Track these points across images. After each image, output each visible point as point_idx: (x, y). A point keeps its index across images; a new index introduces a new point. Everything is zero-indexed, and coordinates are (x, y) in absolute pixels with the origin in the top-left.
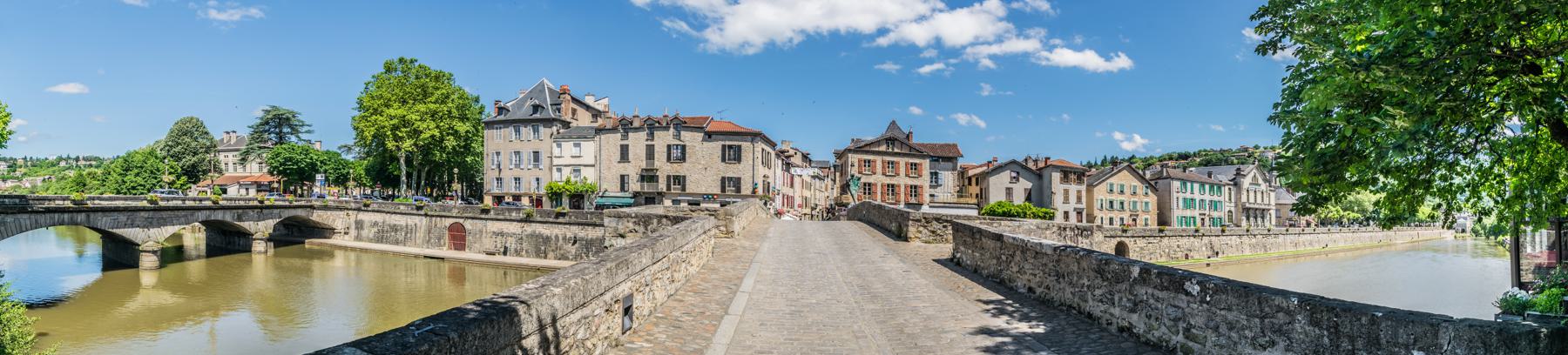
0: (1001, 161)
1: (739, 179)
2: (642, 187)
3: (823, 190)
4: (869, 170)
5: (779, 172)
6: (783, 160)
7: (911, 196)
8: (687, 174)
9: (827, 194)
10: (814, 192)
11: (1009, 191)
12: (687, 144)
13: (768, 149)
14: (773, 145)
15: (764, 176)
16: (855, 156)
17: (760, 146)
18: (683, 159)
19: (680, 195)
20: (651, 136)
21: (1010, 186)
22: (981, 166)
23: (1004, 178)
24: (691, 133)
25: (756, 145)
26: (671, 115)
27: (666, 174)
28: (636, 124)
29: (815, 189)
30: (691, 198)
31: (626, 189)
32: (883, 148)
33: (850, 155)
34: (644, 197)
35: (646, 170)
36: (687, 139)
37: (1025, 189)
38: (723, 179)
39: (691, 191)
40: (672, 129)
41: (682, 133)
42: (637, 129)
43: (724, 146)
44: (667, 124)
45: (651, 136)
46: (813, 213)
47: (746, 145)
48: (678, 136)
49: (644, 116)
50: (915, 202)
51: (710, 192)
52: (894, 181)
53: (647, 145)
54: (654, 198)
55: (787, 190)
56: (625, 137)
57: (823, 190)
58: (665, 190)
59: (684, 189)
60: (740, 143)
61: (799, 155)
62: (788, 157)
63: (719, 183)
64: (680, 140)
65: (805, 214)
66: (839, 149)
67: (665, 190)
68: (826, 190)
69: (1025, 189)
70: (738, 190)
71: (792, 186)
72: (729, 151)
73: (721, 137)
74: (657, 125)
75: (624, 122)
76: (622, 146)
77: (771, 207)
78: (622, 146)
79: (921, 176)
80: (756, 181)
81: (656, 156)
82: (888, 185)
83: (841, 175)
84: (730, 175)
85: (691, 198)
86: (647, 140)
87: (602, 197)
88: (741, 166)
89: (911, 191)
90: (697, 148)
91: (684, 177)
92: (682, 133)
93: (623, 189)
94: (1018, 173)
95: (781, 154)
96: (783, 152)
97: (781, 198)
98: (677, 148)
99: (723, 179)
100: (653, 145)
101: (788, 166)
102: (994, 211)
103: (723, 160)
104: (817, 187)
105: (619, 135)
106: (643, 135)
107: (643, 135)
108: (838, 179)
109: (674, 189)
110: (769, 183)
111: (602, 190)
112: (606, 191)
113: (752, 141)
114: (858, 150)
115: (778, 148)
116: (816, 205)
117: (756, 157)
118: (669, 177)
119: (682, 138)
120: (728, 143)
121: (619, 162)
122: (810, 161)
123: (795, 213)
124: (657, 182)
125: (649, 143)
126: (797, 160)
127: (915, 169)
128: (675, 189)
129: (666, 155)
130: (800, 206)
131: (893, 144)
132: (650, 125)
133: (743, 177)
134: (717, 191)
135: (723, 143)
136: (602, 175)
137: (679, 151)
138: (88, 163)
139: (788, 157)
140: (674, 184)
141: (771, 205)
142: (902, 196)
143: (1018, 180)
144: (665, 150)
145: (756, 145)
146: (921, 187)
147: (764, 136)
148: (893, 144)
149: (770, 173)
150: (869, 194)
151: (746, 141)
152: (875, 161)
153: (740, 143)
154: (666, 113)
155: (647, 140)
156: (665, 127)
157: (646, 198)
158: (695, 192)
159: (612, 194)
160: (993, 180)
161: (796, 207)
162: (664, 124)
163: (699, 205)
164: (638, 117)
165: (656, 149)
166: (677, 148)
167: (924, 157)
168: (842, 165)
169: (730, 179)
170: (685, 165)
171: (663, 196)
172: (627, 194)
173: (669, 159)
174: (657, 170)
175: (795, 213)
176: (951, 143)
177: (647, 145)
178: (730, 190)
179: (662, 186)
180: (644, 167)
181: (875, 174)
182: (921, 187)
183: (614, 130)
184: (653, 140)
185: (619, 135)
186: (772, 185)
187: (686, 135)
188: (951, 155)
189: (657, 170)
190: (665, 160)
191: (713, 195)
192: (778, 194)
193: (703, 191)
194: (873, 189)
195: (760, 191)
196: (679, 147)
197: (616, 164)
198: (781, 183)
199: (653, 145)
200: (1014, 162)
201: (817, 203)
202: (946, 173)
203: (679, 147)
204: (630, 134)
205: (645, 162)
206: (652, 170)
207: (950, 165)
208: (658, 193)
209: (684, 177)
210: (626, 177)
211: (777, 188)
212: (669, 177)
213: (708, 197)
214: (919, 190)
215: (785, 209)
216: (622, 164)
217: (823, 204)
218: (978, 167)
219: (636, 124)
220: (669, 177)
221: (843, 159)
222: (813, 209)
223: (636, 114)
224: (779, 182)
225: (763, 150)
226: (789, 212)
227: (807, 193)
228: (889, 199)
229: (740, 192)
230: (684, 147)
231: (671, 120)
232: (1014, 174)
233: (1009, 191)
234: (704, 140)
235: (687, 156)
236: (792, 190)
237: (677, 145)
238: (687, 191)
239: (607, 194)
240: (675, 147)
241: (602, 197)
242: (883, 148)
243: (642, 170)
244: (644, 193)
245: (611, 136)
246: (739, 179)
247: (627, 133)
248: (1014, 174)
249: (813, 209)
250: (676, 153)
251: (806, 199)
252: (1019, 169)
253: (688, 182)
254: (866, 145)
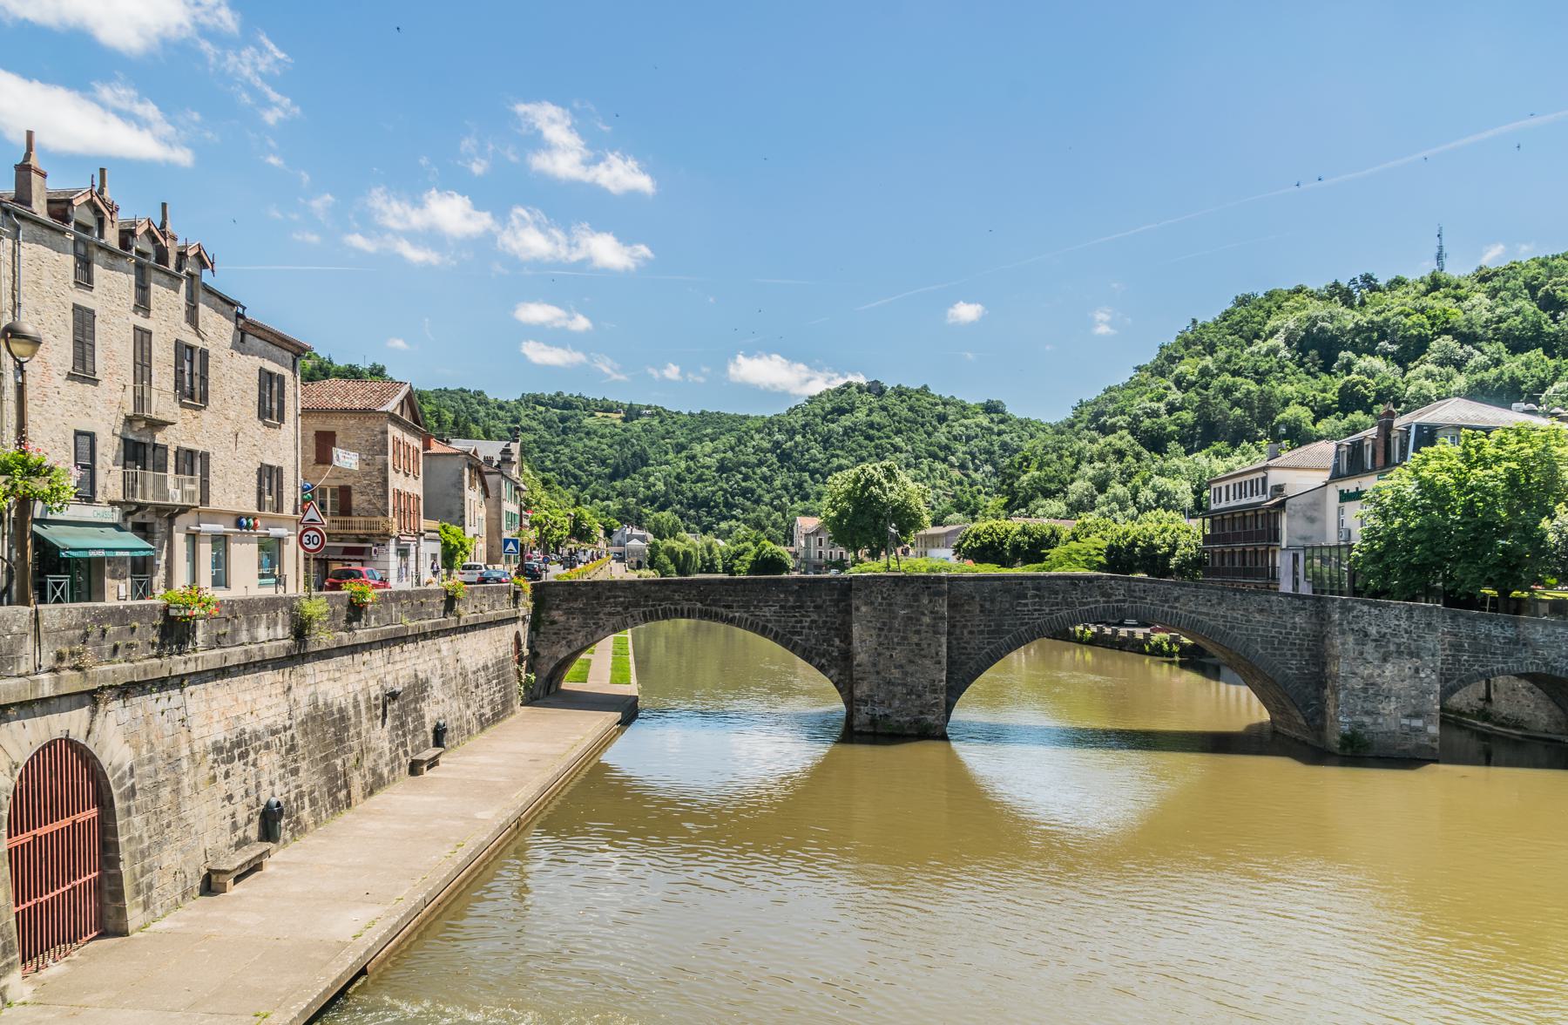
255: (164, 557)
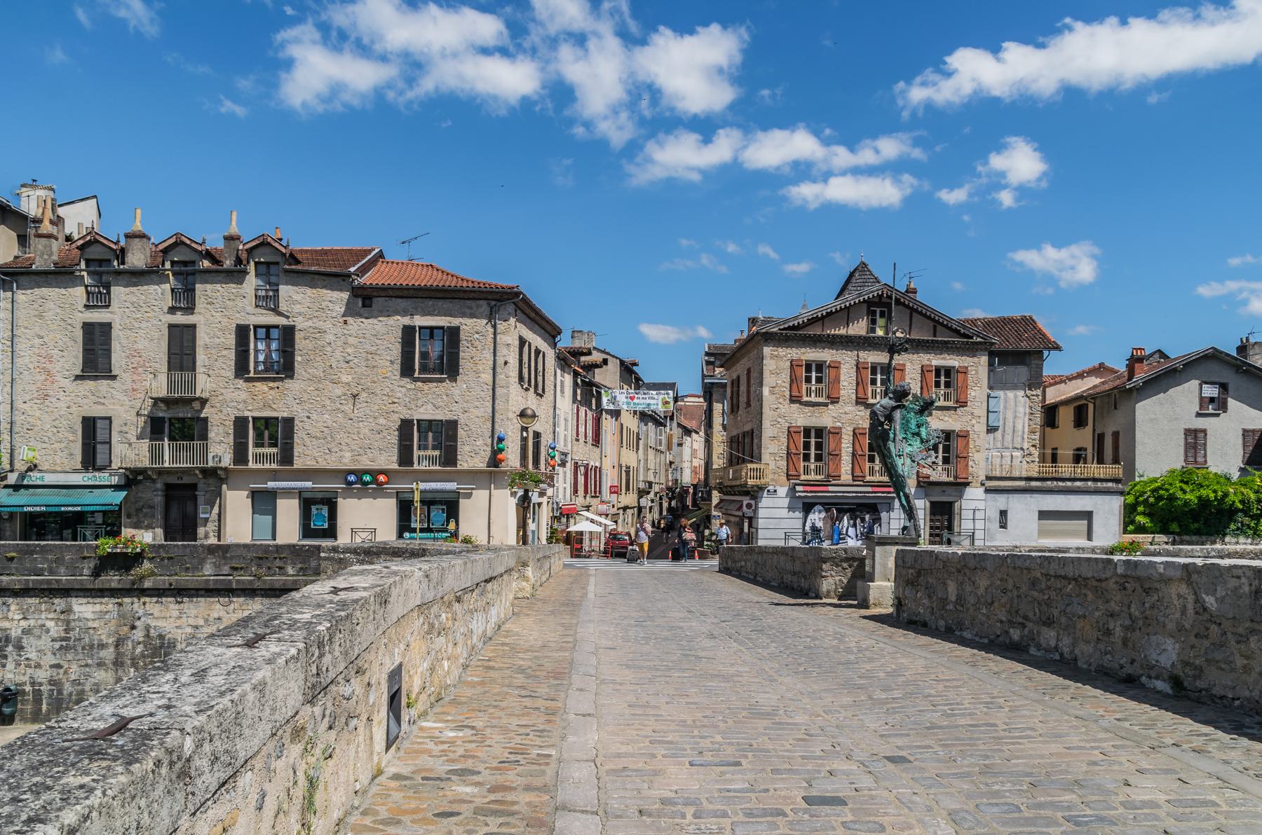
0: (1179, 349)
1: (452, 425)
2: (156, 454)
3: (663, 448)
4: (819, 393)
5: (565, 404)
6: (576, 374)
7: (806, 458)
8: (298, 412)
9: (669, 458)
10: (646, 454)
11: (1195, 441)
12: (300, 323)
13: (537, 341)
14: (551, 331)
15: (523, 414)
16: (782, 351)
17: (513, 330)
18: (285, 367)
19: (275, 475)
20: (185, 299)
21: (1200, 423)
22: (1080, 376)
23: (1186, 395)
24: (309, 291)
25: (501, 326)
26: (249, 236)
27: (234, 413)
28: (137, 258)
29: (646, 446)
30: (309, 484)
31: (100, 461)
32: (859, 328)
33: (767, 350)
34: (159, 485)
35: (167, 402)
36: (297, 308)
37: (1246, 432)
38: (406, 427)
39: (311, 464)
40: (252, 281)
41: (284, 290)
42: (138, 277)
43: (408, 332)
44: (239, 261)
45: (185, 299)
46: (643, 502)
47: (472, 327)
48: (269, 301)
49: (160, 235)
50: (944, 478)
51: (365, 463)
52: (826, 418)
53: (172, 327)
54: (194, 487)
55: (584, 453)
56: (99, 299)
57: (663, 448)
58: (227, 461)
59: (287, 457)
60: (455, 322)
61: (613, 368)
62: (591, 367)
63: (394, 439)
64: (276, 310)
65: (625, 508)
66: (720, 342)
67: (227, 461)
68: (669, 448)
69: (1246, 432)
70: (450, 457)
71: (597, 440)
72: (746, 744)
73: (402, 303)
74: (206, 264)
75: (94, 252)
76: (88, 327)
77: (544, 500)
78: (88, 327)
79: (964, 404)
80: (500, 430)
81: (201, 358)
82: (807, 431)
83: (734, 409)
84: (426, 412)
85: (309, 484)
86: (172, 310)
87: (16, 487)
88: (457, 389)
89: (807, 446)
90: (330, 337)
91: (289, 422)
92: (284, 290)
93: (90, 461)
94: (1224, 387)
95: (567, 359)
96: (577, 353)
97: (569, 475)
98: (268, 336)
99: (406, 427)
100: (194, 327)
101: (588, 392)
102: (1172, 498)
103: (407, 370)
104: (652, 443)
105: (80, 292)
106: (160, 294)
107: (160, 294)
108: (717, 420)
109: (258, 458)
110: (537, 435)
111: (20, 466)
112: (33, 467)
113: (491, 317)
114: (792, 334)
115: (565, 342)
116: (650, 484)
117: (500, 361)
118: (240, 423)
119: (283, 307)
120: (419, 321)
121: (78, 378)
122: (638, 379)
123: (603, 508)
124: (204, 436)
125: (180, 318)
126: (608, 376)
127: (948, 385)
128: (260, 457)
129: (232, 355)
130: (615, 490)
131: (887, 316)
132: (185, 263)
133: (461, 422)
134: (388, 459)
135: (406, 321)
136: (18, 418)
137: (274, 345)
138: (813, 452)
139: (591, 367)
140: (258, 444)
141: (542, 494)
142: (846, 459)
143: (1223, 406)
144: (231, 340)
145: (501, 326)
146: (965, 435)
147: (526, 301)
148: (887, 316)
149: (540, 407)
150: (819, 458)
151: (472, 316)
152: (836, 366)
153: (455, 322)
154: (234, 229)
155: (172, 310)
156: (229, 272)
157: (169, 487)
158: (323, 464)
159: (50, 479)
160: (1146, 410)
161: (606, 494)
162: (228, 263)
163: (972, 338)
164: (142, 236)
165: (202, 338)
166: (268, 336)
167: (970, 348)
168: (736, 383)
169: (428, 426)
170: (293, 386)
171: (222, 481)
172: (103, 478)
173: (241, 368)
174: (203, 402)
175: (603, 508)
176: (1017, 314)
177: (171, 326)
178: (425, 458)
179: (220, 450)
180: (163, 393)
181: (835, 400)
182: (965, 435)
183: (61, 275)
184: (190, 309)
185: (80, 292)
186: (546, 440)
187: (296, 299)
188: (1024, 345)
189: (203, 402)
190: (230, 373)
191: (374, 473)
192: (563, 464)
193: (345, 460)
194: (829, 445)
195: (512, 458)
196: (275, 334)
197: (67, 383)
198: (571, 433)
199: (194, 327)
200: (1213, 356)
201: (651, 478)
202: (1010, 394)
203: (275, 334)
204: (118, 292)
205: (163, 378)
206: (188, 402)
207: (1022, 372)
208: (206, 472)
209: (289, 422)
210: (99, 424)
211: (560, 446)
212: (240, 424)
213: (360, 481)
214: (957, 444)
215: (580, 501)
216: (90, 384)
217: (663, 481)
218: (1071, 378)
219: (137, 258)
220: (240, 424)
221: (740, 369)
222: (642, 493)
223: (138, 226)
224: (565, 432)
225: (522, 341)
226: (588, 508)
227: (630, 458)
228: (872, 472)
229: (291, 462)
230: (288, 334)
231: (250, 251)
232: (1211, 391)
233: (1195, 441)
234: (350, 311)
235: (298, 358)
236: (598, 450)
237: (268, 328)
238: (298, 463)
239: (35, 478)
240: (262, 332)
241: (16, 487)
242: (859, 328)
243: (156, 401)
244: (162, 472)
245: (52, 295)
246: (452, 425)
247: (108, 287)
248: (1211, 391)
249: (642, 493)
250: (259, 351)
251: (628, 473)
252: (1227, 376)
253: (299, 437)
254: (813, 321)
255: (216, 510)
